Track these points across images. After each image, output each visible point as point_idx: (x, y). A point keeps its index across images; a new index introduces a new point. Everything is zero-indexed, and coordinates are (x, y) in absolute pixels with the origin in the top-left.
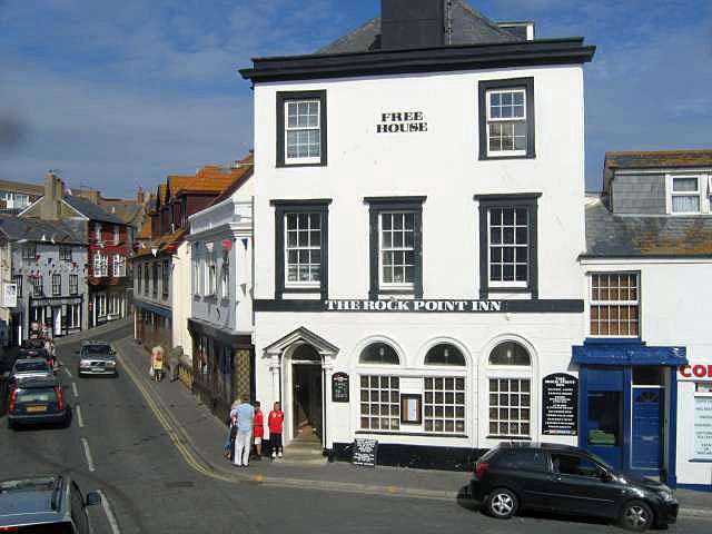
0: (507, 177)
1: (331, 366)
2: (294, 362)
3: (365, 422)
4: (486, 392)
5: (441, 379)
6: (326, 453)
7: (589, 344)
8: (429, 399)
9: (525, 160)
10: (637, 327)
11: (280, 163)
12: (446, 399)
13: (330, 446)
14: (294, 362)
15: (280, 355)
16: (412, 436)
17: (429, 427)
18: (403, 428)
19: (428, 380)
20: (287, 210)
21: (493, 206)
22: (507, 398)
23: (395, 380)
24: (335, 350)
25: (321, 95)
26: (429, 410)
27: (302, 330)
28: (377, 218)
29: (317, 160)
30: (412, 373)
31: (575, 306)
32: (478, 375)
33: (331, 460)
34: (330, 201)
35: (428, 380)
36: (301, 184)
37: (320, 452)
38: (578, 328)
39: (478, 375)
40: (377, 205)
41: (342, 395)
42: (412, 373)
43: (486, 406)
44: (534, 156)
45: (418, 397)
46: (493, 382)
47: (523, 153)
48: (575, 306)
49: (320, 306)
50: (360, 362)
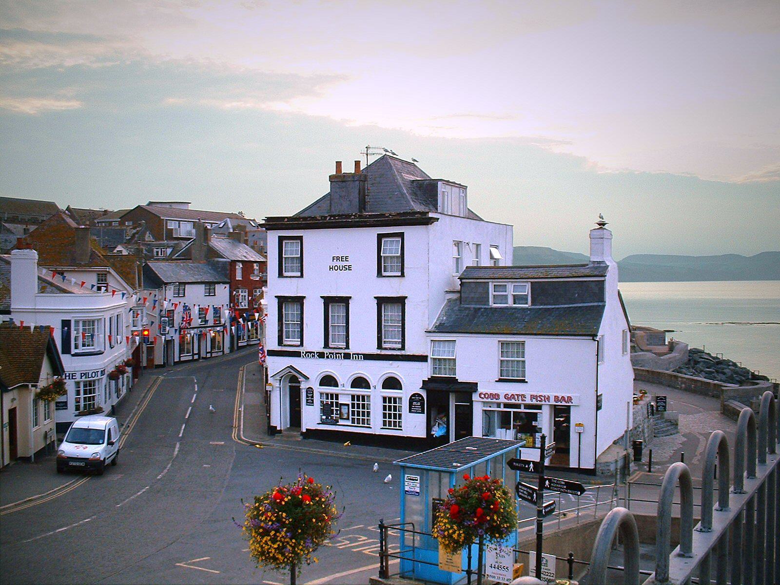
0: (390, 288)
1: (304, 386)
2: (290, 384)
3: (384, 423)
4: (380, 404)
5: (391, 398)
6: (302, 434)
7: (432, 380)
8: (353, 407)
9: (400, 278)
10: (453, 370)
11: (281, 275)
12: (360, 405)
13: (304, 431)
14: (290, 384)
15: (280, 380)
16: (345, 426)
17: (353, 422)
18: (341, 422)
19: (353, 397)
20: (282, 301)
21: (381, 301)
22: (391, 408)
23: (337, 396)
24: (307, 378)
25: (300, 238)
26: (353, 412)
27: (291, 367)
28: (381, 307)
29: (399, 274)
30: (345, 393)
31: (423, 359)
32: (376, 395)
33: (304, 438)
34: (350, 297)
35: (353, 397)
36: (289, 288)
37: (299, 433)
38: (424, 371)
39: (376, 395)
40: (328, 301)
41: (310, 402)
42: (345, 393)
43: (381, 411)
44: (303, 277)
45: (348, 405)
46: (384, 399)
47: (399, 274)
48: (423, 359)
49: (297, 354)
50: (352, 387)
